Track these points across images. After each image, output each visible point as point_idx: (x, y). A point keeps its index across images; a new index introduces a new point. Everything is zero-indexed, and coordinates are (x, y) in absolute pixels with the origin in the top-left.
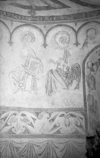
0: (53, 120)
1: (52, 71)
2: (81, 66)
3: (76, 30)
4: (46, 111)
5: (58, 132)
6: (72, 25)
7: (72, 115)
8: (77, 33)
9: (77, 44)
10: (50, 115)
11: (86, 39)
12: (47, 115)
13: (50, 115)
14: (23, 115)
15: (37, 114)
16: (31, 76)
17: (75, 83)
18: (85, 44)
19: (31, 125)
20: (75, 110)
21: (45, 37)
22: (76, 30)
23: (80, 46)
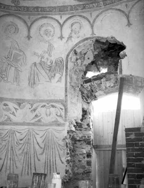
0: (35, 110)
1: (35, 64)
2: (64, 59)
3: (62, 22)
4: (28, 101)
5: (39, 121)
6: (57, 17)
7: (53, 106)
8: (61, 26)
9: (61, 38)
10: (32, 105)
11: (71, 33)
12: (29, 106)
13: (32, 105)
14: (5, 105)
15: (19, 104)
16: (13, 68)
17: (58, 76)
18: (70, 37)
19: (13, 114)
20: (56, 101)
21: (29, 29)
22: (62, 22)
23: (64, 40)
